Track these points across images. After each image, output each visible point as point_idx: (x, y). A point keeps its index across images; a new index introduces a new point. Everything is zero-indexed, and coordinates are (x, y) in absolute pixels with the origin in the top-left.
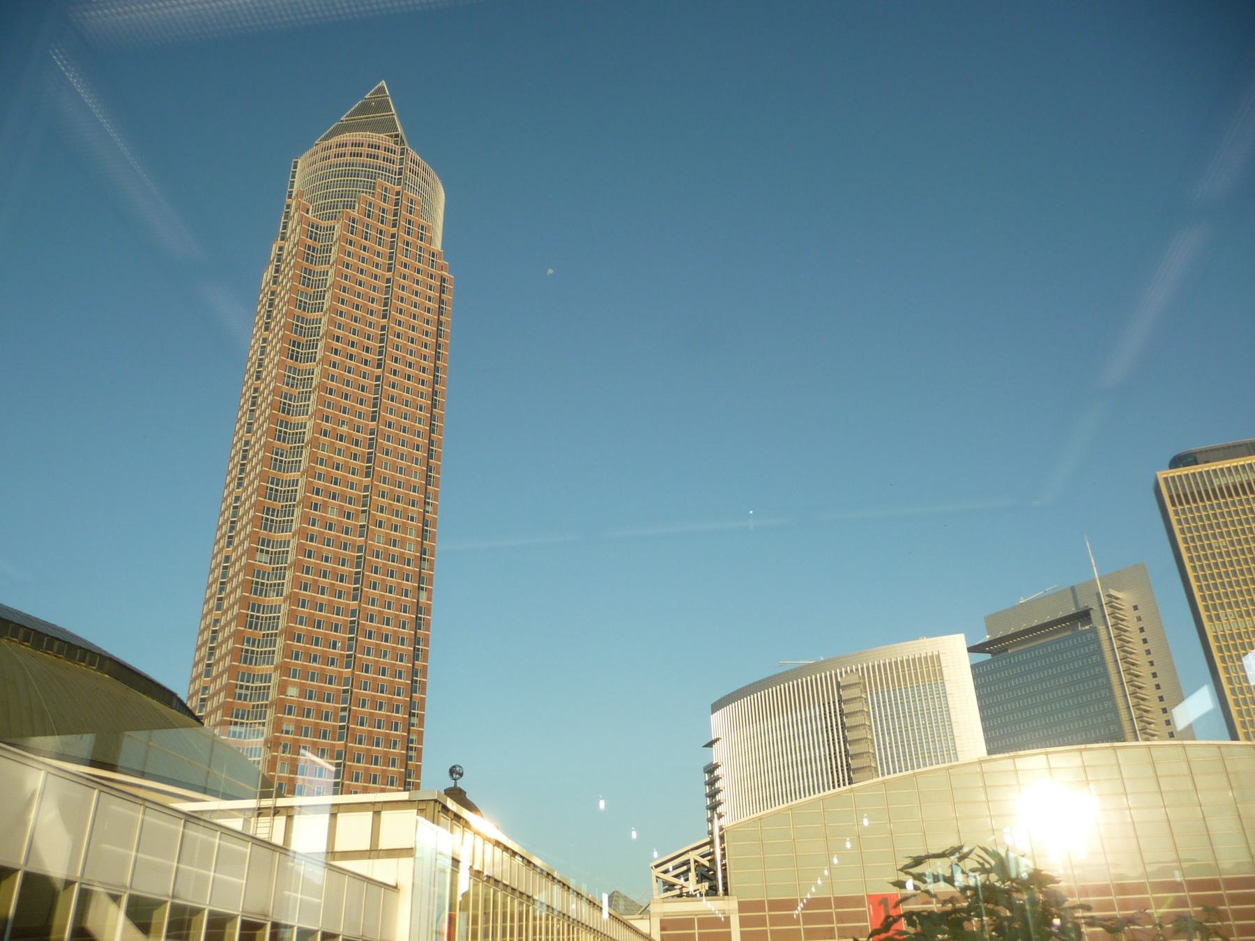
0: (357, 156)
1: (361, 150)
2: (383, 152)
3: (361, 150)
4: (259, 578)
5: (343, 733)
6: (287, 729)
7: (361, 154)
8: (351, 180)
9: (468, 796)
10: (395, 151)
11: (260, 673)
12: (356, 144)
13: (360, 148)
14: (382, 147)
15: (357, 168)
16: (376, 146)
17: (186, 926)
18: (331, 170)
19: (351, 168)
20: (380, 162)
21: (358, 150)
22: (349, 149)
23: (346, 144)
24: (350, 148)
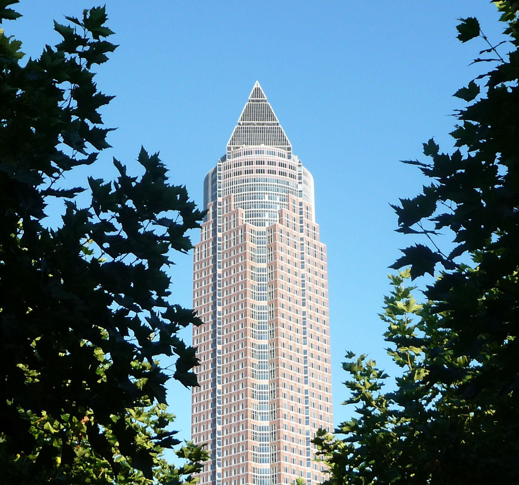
22: (243, 168)
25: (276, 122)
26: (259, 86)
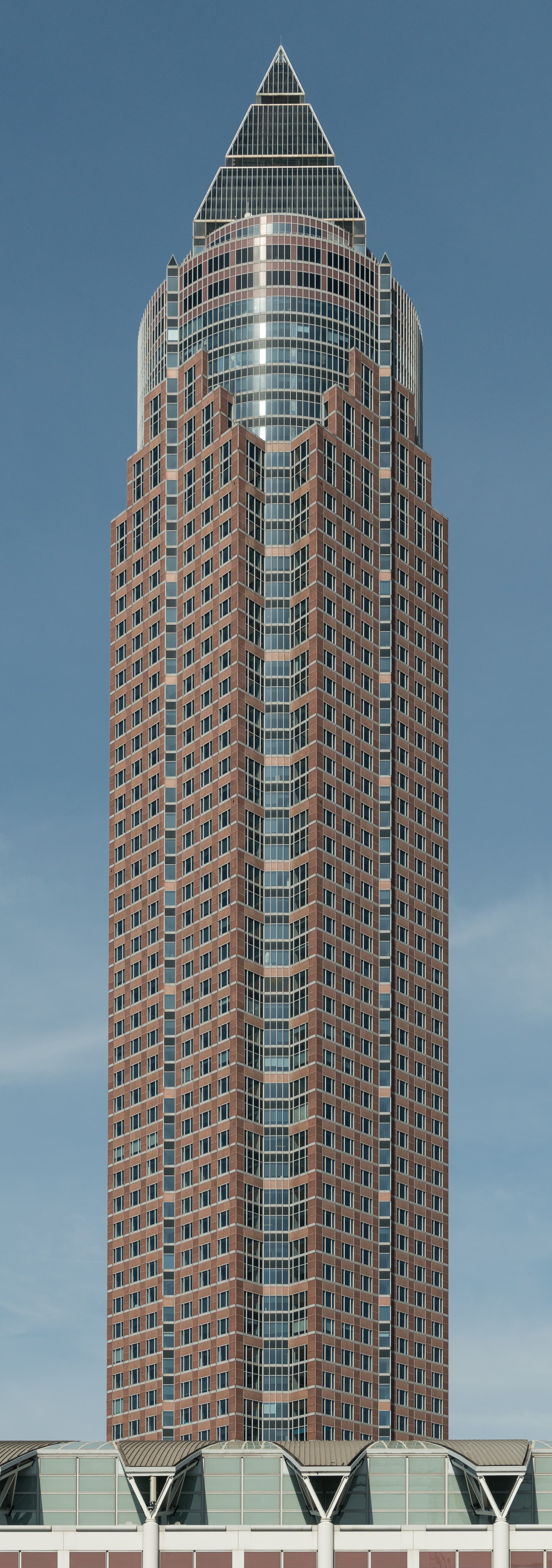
22: (209, 278)
25: (328, 155)
26: (286, 59)
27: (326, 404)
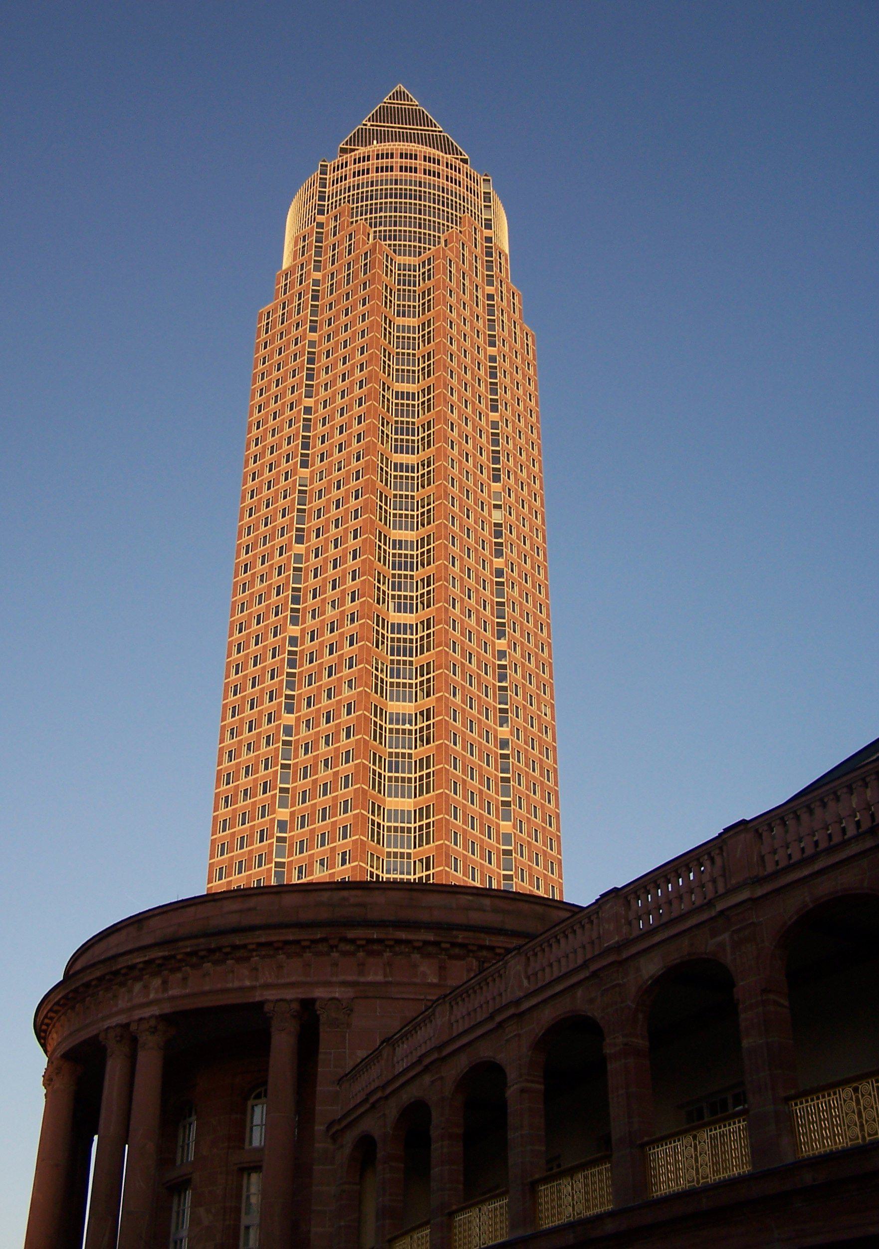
0: (387, 171)
1: (392, 162)
2: (423, 162)
3: (392, 162)
4: (407, 185)
5: (713, 1164)
6: (403, 390)
7: (392, 154)
8: (381, 190)
9: (748, 819)
10: (439, 173)
11: (405, 391)
12: (382, 154)
13: (389, 173)
14: (420, 169)
15: (389, 187)
16: (411, 155)
17: (440, 1148)
18: (351, 193)
19: (383, 201)
20: (420, 175)
21: (387, 162)
22: (373, 162)
23: (369, 156)
24: (375, 161)
27: (446, 241)
